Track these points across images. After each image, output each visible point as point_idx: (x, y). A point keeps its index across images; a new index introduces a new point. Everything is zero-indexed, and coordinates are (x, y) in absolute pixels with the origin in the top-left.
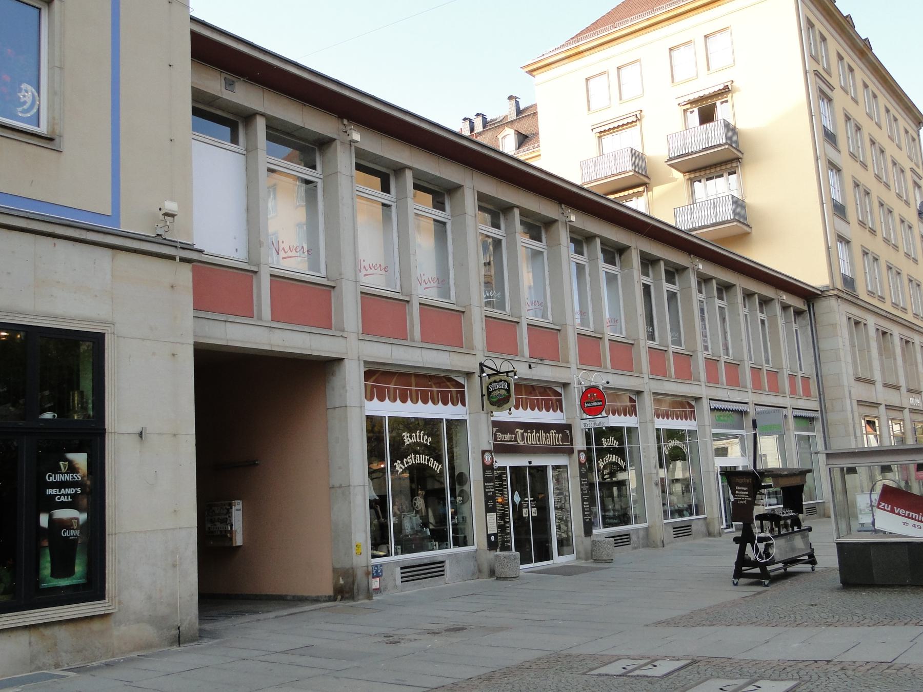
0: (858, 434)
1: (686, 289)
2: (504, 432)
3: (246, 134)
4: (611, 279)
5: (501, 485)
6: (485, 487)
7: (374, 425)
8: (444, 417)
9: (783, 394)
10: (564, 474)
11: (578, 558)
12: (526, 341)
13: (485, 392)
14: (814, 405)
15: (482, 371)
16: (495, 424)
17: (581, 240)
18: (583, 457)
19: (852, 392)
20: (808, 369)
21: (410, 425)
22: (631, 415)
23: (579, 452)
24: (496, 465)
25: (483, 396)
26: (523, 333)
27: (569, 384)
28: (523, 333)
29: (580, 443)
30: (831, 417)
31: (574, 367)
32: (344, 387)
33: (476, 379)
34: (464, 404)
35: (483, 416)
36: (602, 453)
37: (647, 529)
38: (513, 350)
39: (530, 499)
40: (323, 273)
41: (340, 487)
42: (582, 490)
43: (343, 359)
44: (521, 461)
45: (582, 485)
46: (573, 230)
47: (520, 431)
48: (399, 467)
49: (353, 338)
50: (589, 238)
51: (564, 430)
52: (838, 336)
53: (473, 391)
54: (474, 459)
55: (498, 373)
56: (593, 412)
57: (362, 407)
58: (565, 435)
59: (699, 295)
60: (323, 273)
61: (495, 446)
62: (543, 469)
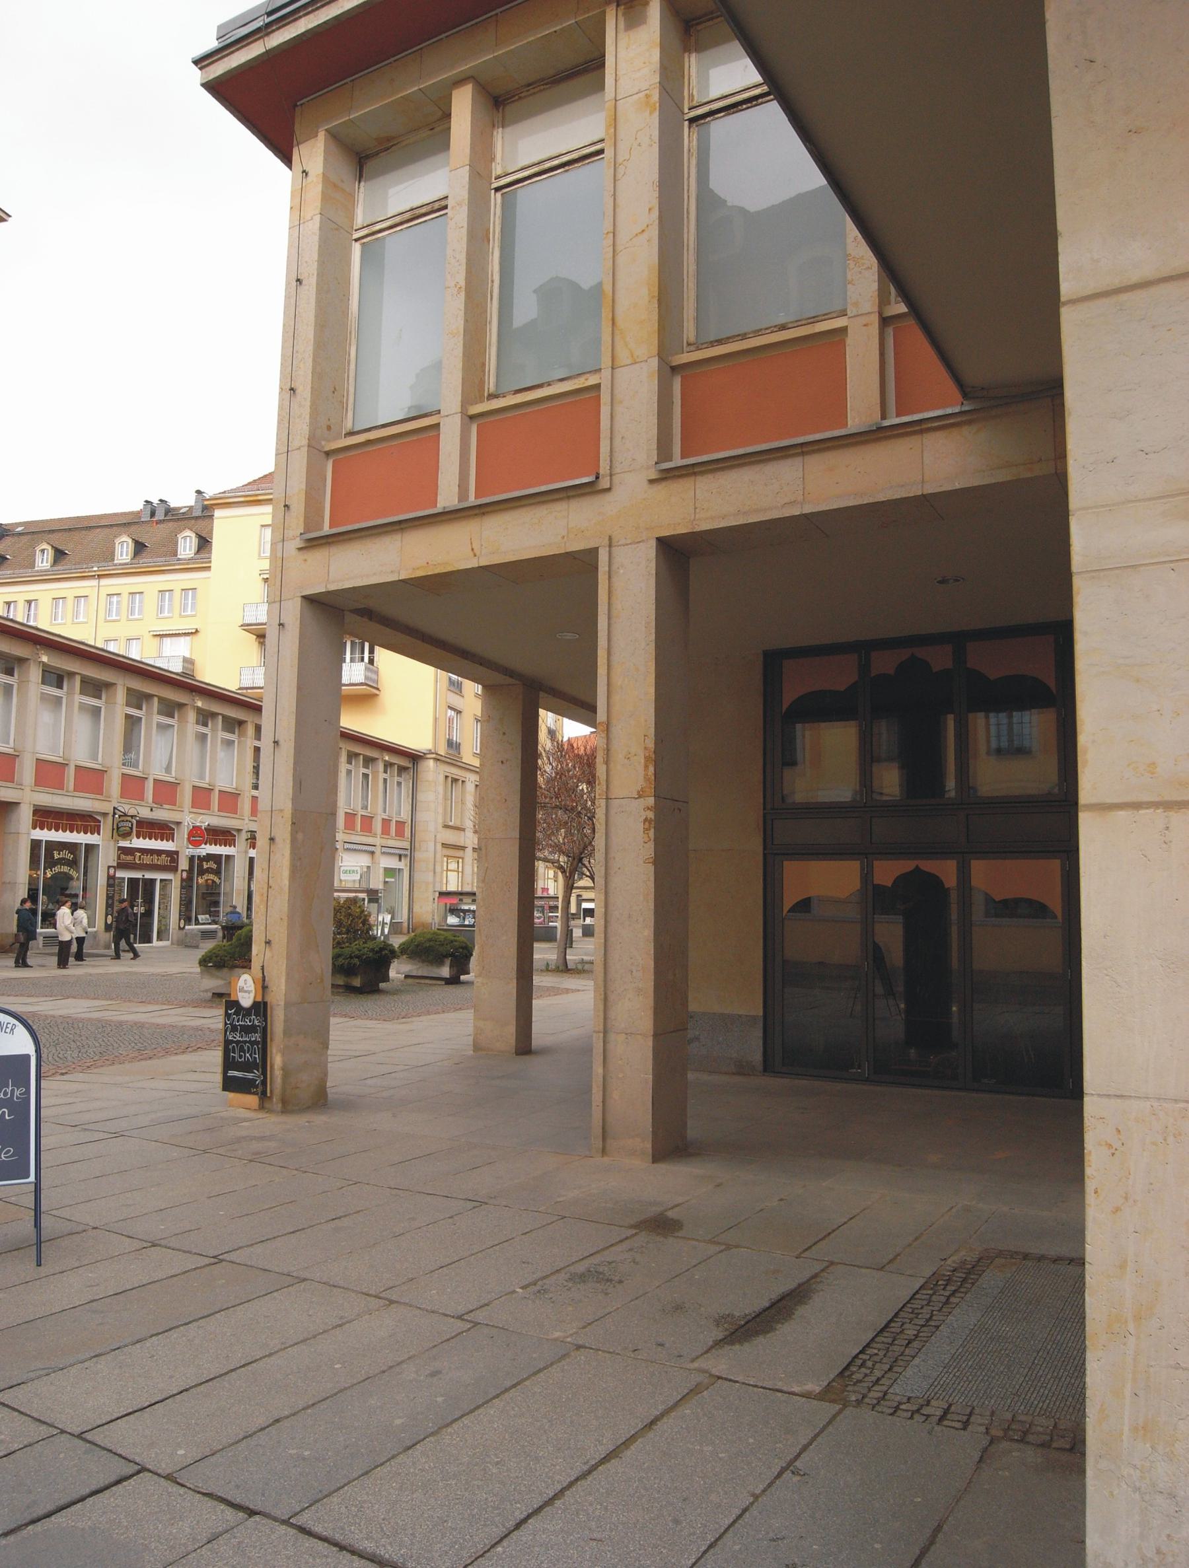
0: (438, 869)
1: (375, 773)
2: (126, 854)
3: (19, 672)
4: (202, 738)
5: (121, 890)
6: (107, 890)
7: (35, 844)
8: (224, 854)
9: (375, 836)
10: (169, 886)
11: (172, 944)
12: (151, 792)
13: (115, 827)
14: (406, 845)
15: (115, 814)
16: (119, 848)
17: (205, 717)
18: (185, 875)
19: (438, 837)
20: (405, 815)
21: (62, 846)
22: (230, 846)
23: (182, 871)
24: (117, 875)
25: (113, 829)
26: (149, 787)
27: (181, 823)
28: (149, 787)
29: (183, 864)
30: (418, 855)
31: (186, 810)
32: (19, 821)
33: (110, 818)
34: (99, 834)
35: (112, 843)
36: (202, 872)
37: (96, 932)
38: (141, 797)
39: (140, 901)
40: (12, 744)
41: (9, 883)
42: (181, 897)
43: (19, 803)
44: (137, 875)
45: (181, 894)
46: (199, 711)
47: (138, 854)
48: (200, 881)
49: (28, 789)
50: (214, 715)
51: (173, 855)
52: (187, 722)
53: (106, 826)
54: (102, 871)
55: (126, 815)
56: (196, 844)
57: (29, 834)
58: (172, 858)
59: (385, 774)
60: (234, 786)
61: (118, 863)
62: (153, 881)
